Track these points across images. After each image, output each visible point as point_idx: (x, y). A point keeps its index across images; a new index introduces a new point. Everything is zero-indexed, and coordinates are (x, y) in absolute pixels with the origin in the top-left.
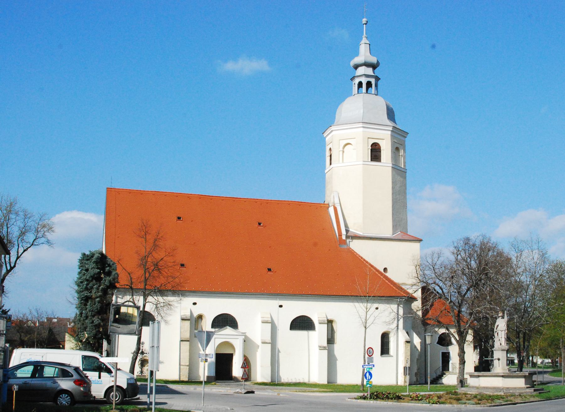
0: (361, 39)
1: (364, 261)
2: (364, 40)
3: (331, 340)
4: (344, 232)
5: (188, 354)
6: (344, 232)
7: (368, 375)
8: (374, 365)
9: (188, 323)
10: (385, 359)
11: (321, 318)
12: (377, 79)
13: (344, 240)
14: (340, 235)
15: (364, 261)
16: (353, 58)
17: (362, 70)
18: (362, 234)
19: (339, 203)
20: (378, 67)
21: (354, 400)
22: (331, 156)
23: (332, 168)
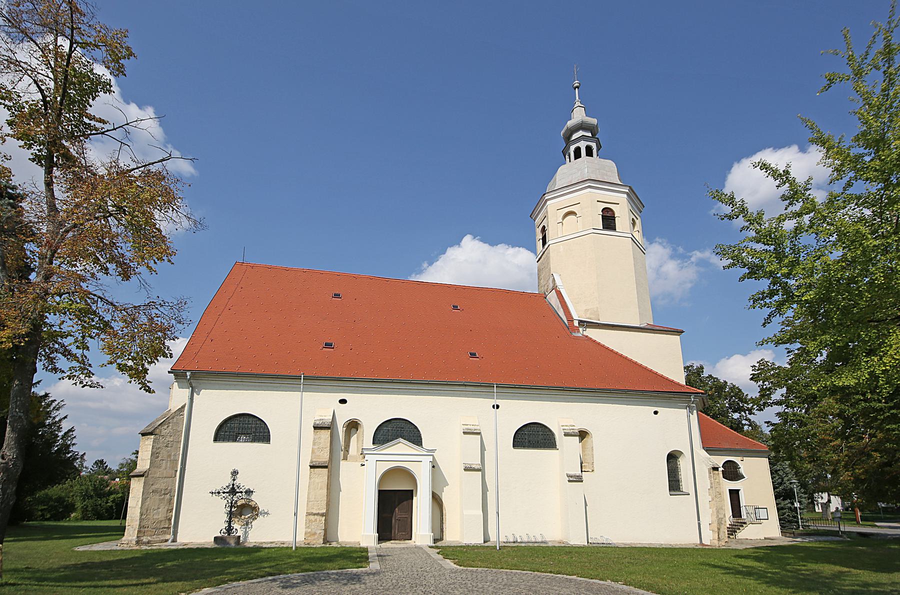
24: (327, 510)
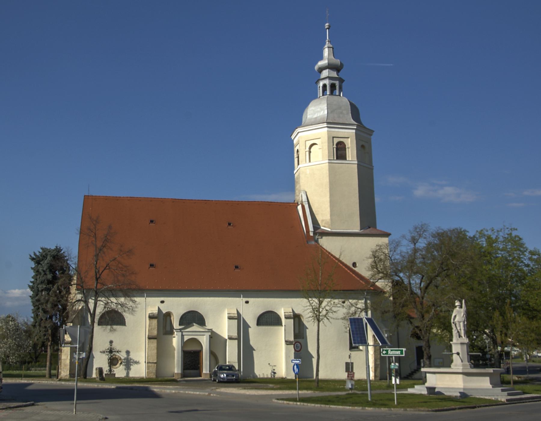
0: (325, 44)
2: (327, 44)
5: (155, 351)
6: (311, 229)
9: (155, 322)
11: (287, 313)
12: (341, 81)
15: (326, 253)
16: (317, 63)
18: (329, 230)
19: (307, 201)
20: (342, 70)
21: (199, 409)
22: (298, 157)
23: (300, 168)
24: (157, 361)
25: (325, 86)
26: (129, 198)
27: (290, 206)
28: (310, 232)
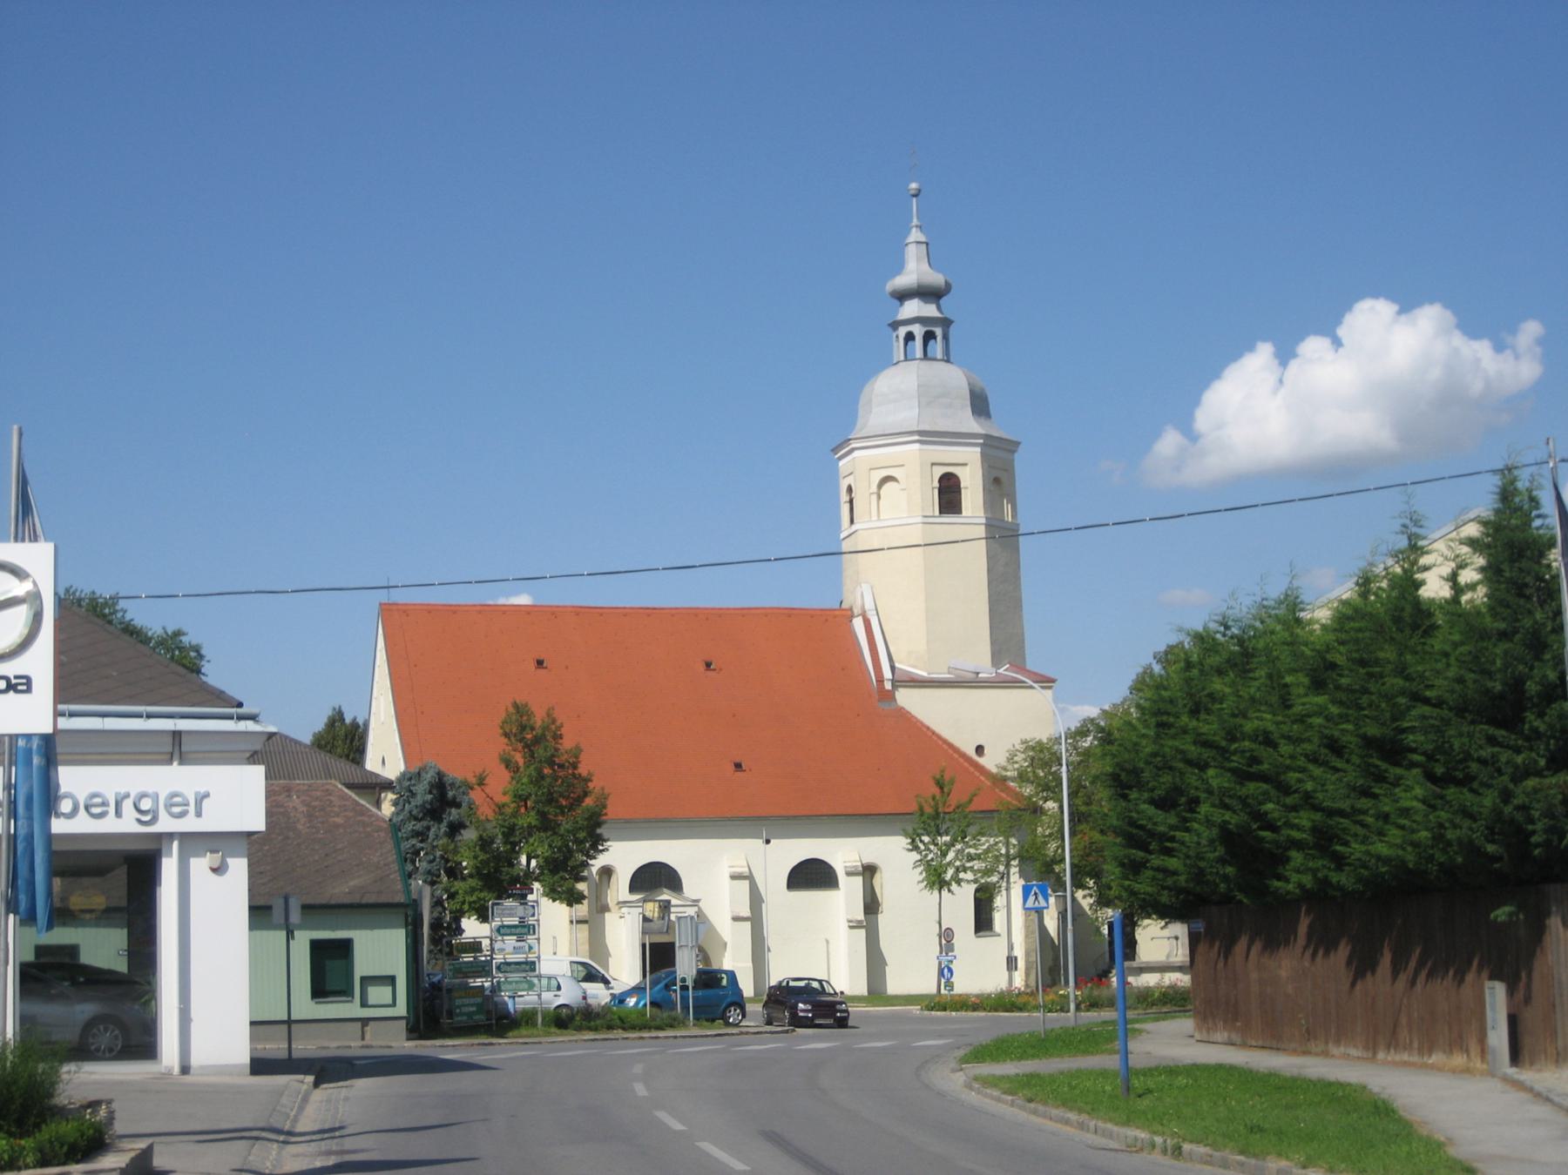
1: (933, 737)
2: (915, 235)
3: (872, 906)
4: (887, 674)
6: (887, 674)
7: (945, 972)
8: (955, 957)
10: (985, 942)
11: (849, 862)
12: (946, 323)
13: (888, 691)
14: (880, 680)
15: (933, 737)
17: (912, 308)
18: (925, 674)
22: (851, 501)
23: (856, 531)
25: (910, 337)
26: (478, 608)
27: (835, 617)
28: (885, 682)
